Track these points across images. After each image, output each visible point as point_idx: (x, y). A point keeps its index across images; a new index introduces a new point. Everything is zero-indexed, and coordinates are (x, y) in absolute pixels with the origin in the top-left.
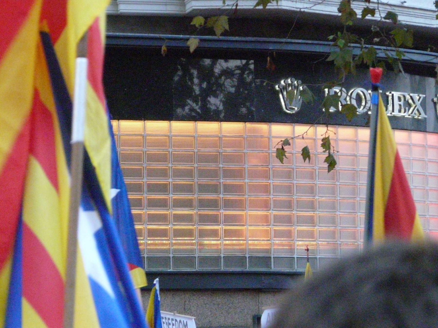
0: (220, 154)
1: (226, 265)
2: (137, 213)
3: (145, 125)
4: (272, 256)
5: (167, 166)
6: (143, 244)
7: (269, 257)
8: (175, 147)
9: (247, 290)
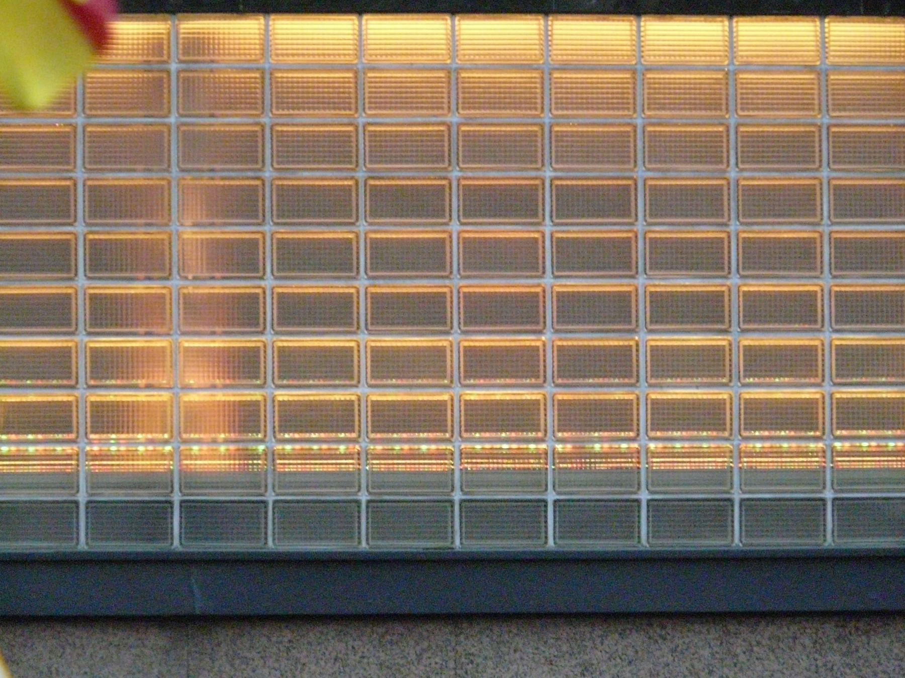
0: (449, 130)
1: (748, 530)
2: (415, 344)
3: (360, 30)
4: (177, 498)
5: (66, 179)
6: (635, 455)
7: (166, 502)
8: (748, 109)
9: (792, 615)
